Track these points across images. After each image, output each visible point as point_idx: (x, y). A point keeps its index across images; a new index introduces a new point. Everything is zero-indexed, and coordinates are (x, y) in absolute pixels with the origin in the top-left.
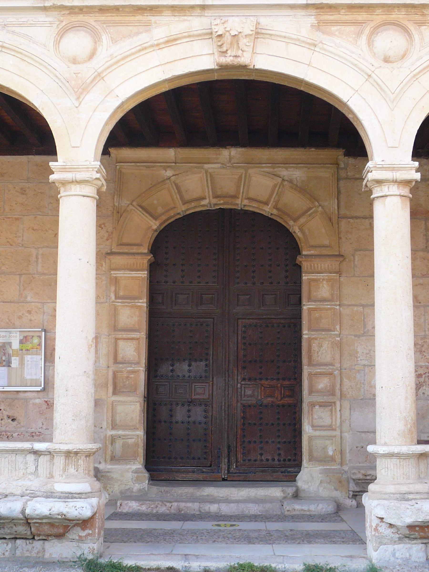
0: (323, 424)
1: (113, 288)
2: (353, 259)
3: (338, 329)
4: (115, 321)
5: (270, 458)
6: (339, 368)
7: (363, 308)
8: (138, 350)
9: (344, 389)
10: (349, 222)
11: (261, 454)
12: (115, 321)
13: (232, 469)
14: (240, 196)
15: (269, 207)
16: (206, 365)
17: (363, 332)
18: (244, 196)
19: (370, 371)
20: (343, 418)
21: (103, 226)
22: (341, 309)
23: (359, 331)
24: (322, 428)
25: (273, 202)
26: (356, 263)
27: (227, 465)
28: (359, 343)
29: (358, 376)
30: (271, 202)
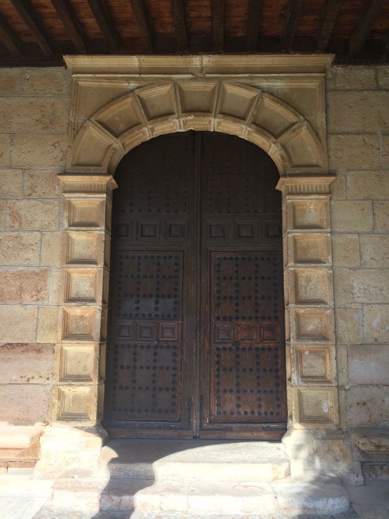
0: (315, 374)
1: (66, 214)
2: (345, 180)
3: (330, 260)
4: (68, 252)
5: (249, 410)
6: (333, 306)
7: (359, 236)
8: (93, 285)
9: (340, 331)
10: (339, 138)
11: (238, 406)
12: (68, 252)
13: (205, 425)
14: (214, 110)
15: (246, 122)
16: (175, 302)
17: (359, 264)
18: (218, 111)
19: (370, 310)
20: (339, 367)
21: (56, 145)
22: (332, 237)
23: (355, 262)
24: (314, 380)
25: (252, 116)
26: (348, 185)
27: (199, 420)
28: (356, 277)
29: (356, 316)
30: (249, 117)
